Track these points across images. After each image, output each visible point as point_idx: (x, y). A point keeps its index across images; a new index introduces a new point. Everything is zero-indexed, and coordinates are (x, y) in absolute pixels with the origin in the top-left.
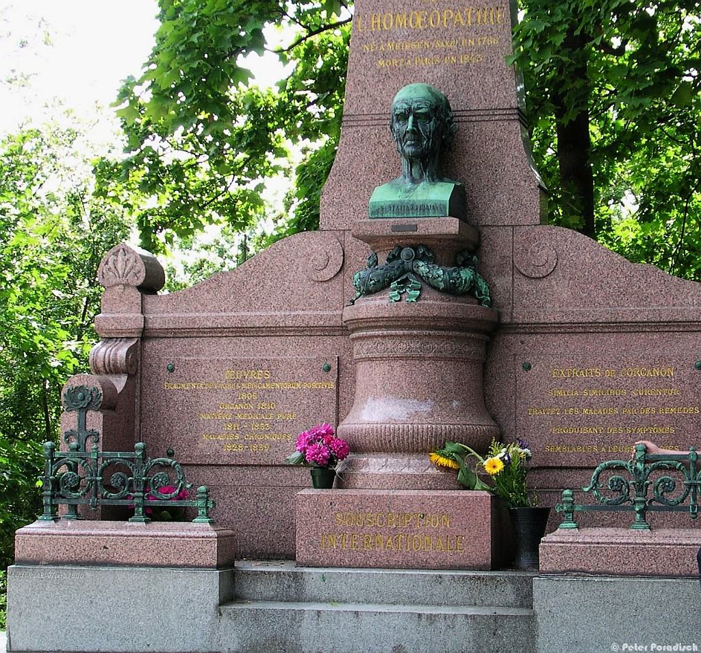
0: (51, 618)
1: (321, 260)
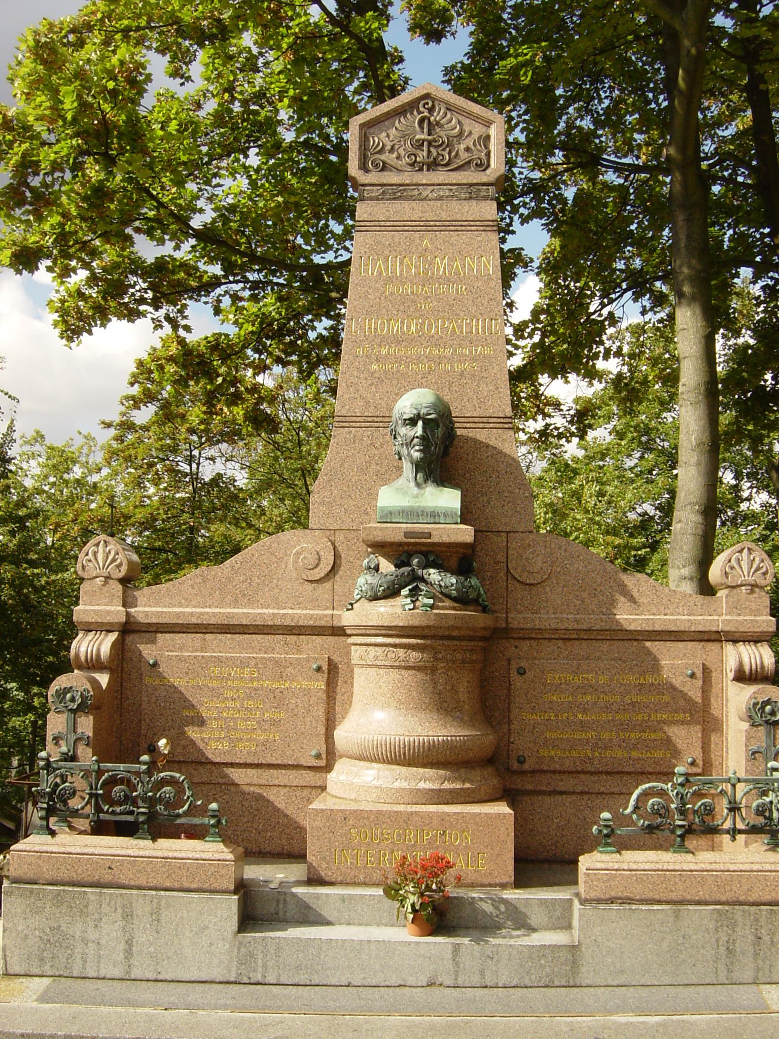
1: (312, 560)
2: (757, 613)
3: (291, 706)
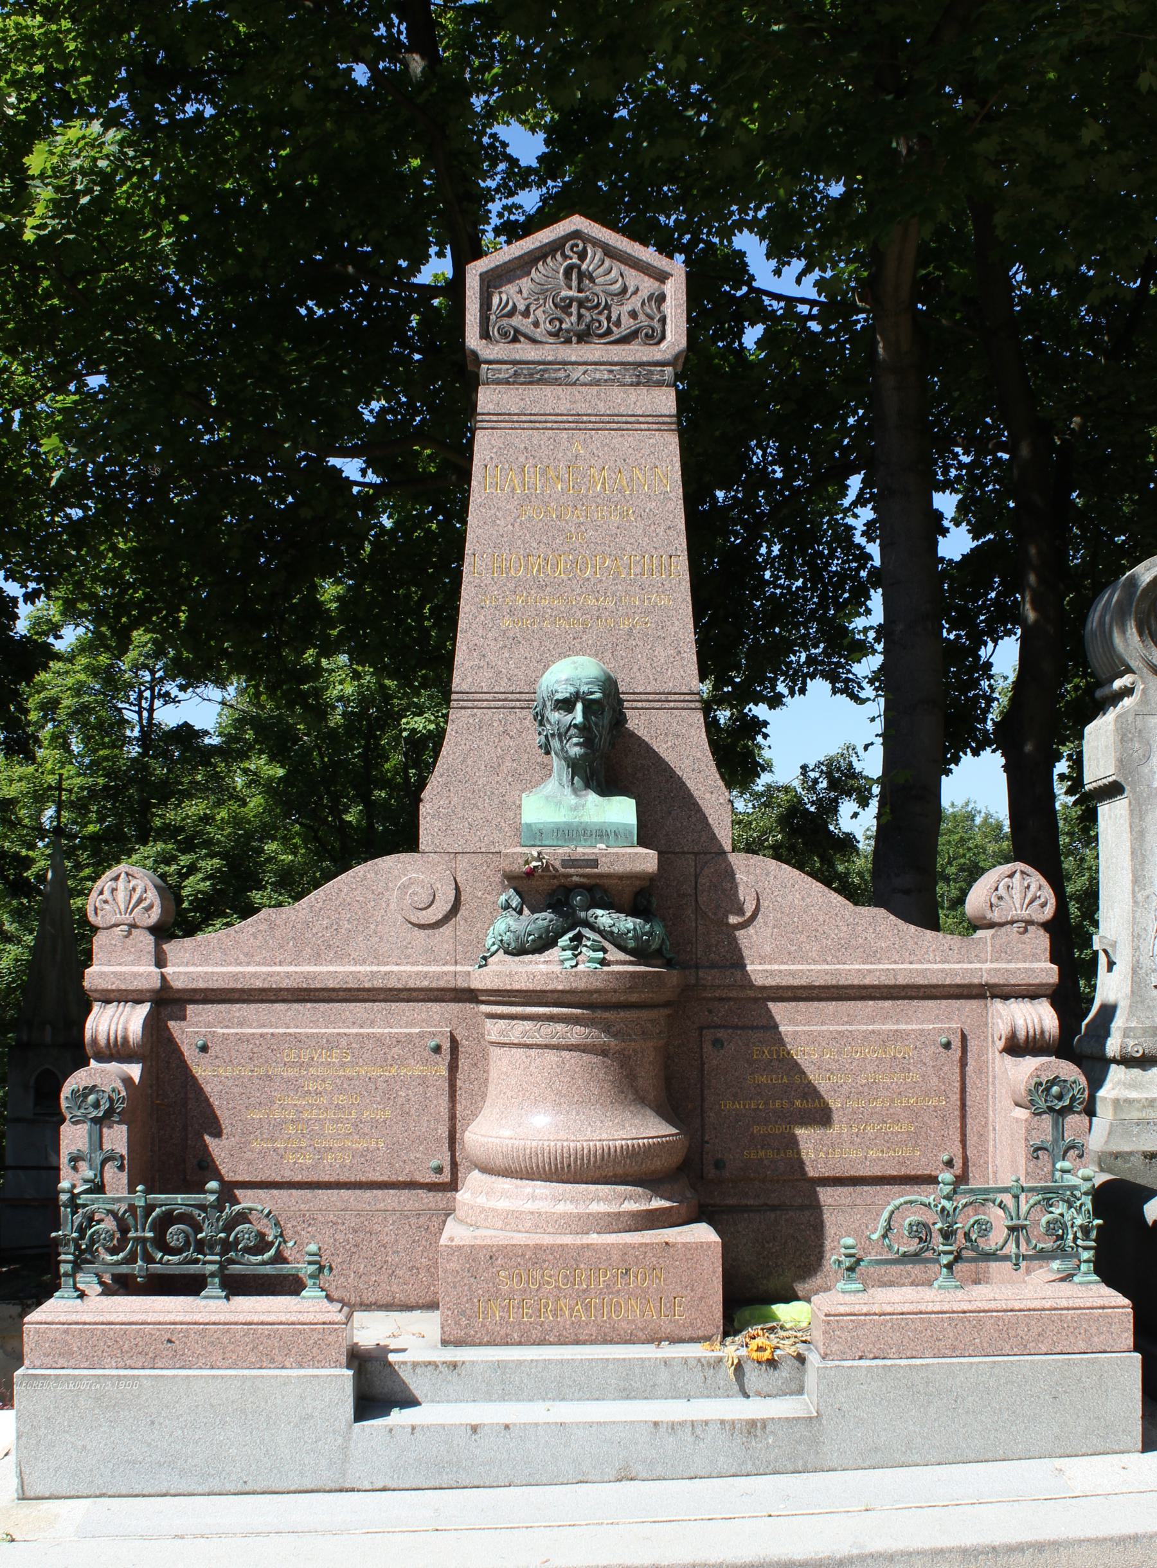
0: (88, 1447)
2: (1035, 958)
3: (400, 1101)
